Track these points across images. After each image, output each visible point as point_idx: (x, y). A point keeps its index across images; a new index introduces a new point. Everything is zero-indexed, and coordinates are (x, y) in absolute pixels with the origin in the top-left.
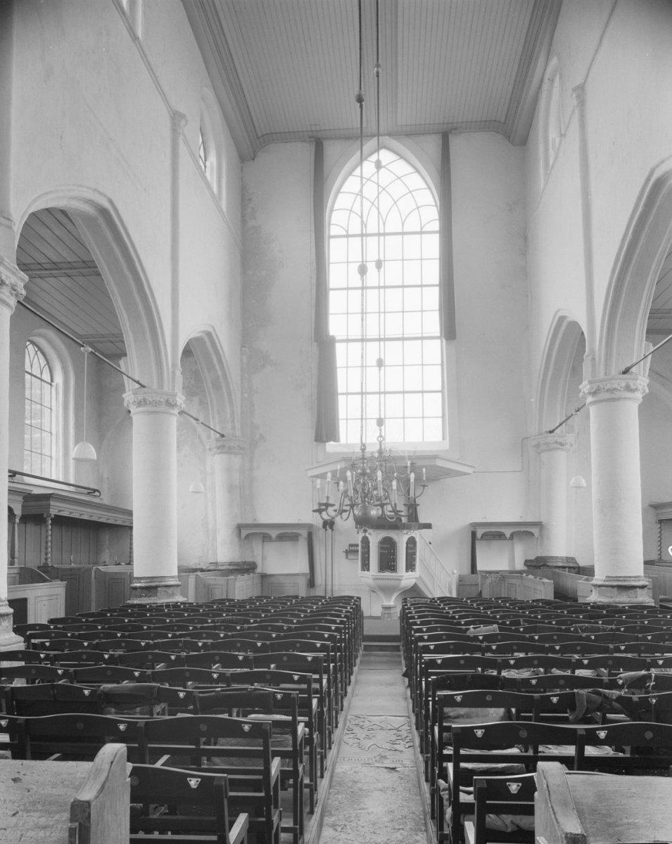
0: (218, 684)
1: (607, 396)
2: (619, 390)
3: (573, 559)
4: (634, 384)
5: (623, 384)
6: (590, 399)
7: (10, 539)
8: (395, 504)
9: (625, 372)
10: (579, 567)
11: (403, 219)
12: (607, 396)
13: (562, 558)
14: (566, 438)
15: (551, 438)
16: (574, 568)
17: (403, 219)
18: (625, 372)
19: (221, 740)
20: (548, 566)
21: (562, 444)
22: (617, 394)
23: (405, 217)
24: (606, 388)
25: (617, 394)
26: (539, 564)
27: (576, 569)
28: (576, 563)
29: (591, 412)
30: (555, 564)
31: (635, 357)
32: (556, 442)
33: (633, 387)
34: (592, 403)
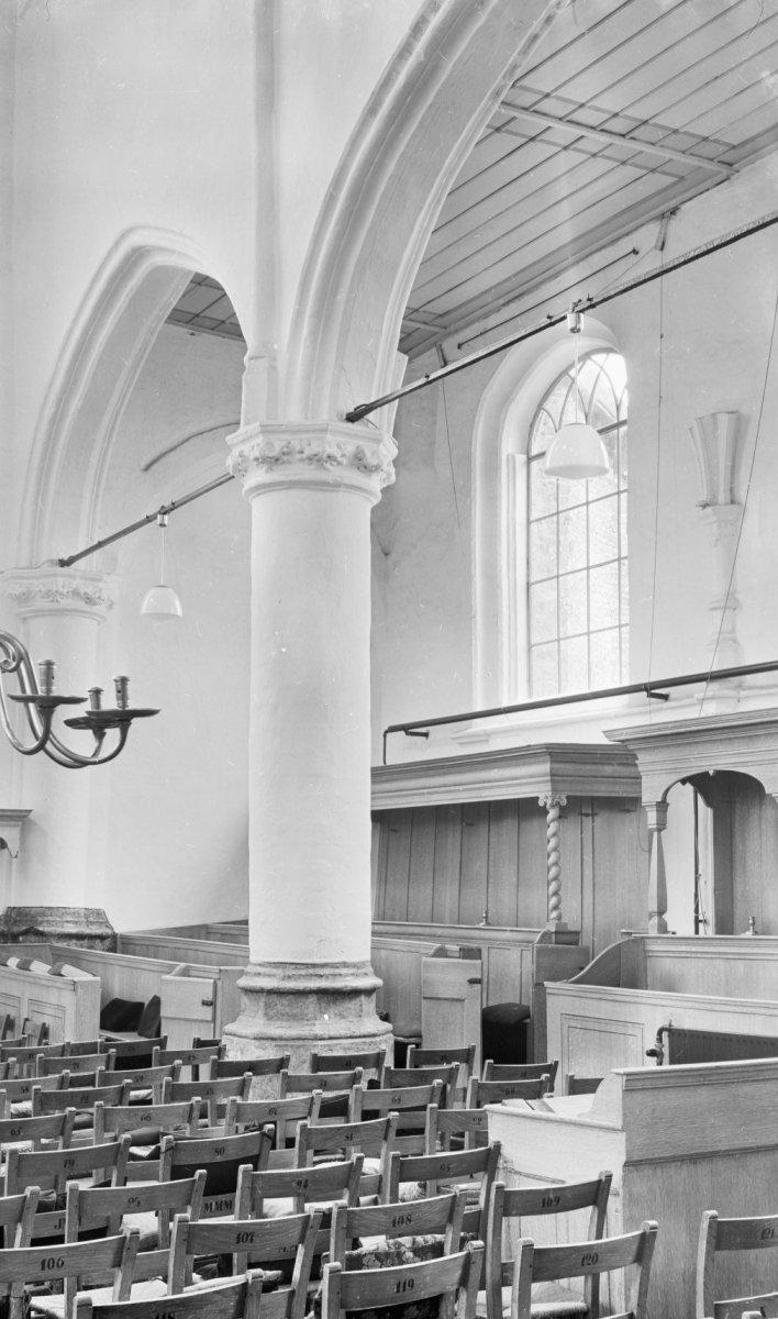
0: (144, 1166)
1: (308, 472)
2: (339, 463)
3: (99, 913)
4: (373, 453)
5: (350, 449)
6: (257, 476)
7: (533, 760)
8: (665, 697)
9: (353, 418)
10: (114, 936)
11: (644, 172)
12: (308, 472)
13: (75, 913)
14: (101, 585)
15: (63, 580)
16: (102, 938)
17: (644, 172)
18: (353, 418)
19: (185, 1289)
20: (42, 934)
21: (89, 600)
22: (333, 473)
23: (611, 162)
24: (307, 452)
25: (333, 473)
26: (15, 929)
27: (107, 942)
28: (109, 926)
29: (255, 512)
30: (60, 930)
31: (374, 392)
32: (76, 593)
33: (371, 460)
34: (261, 488)
